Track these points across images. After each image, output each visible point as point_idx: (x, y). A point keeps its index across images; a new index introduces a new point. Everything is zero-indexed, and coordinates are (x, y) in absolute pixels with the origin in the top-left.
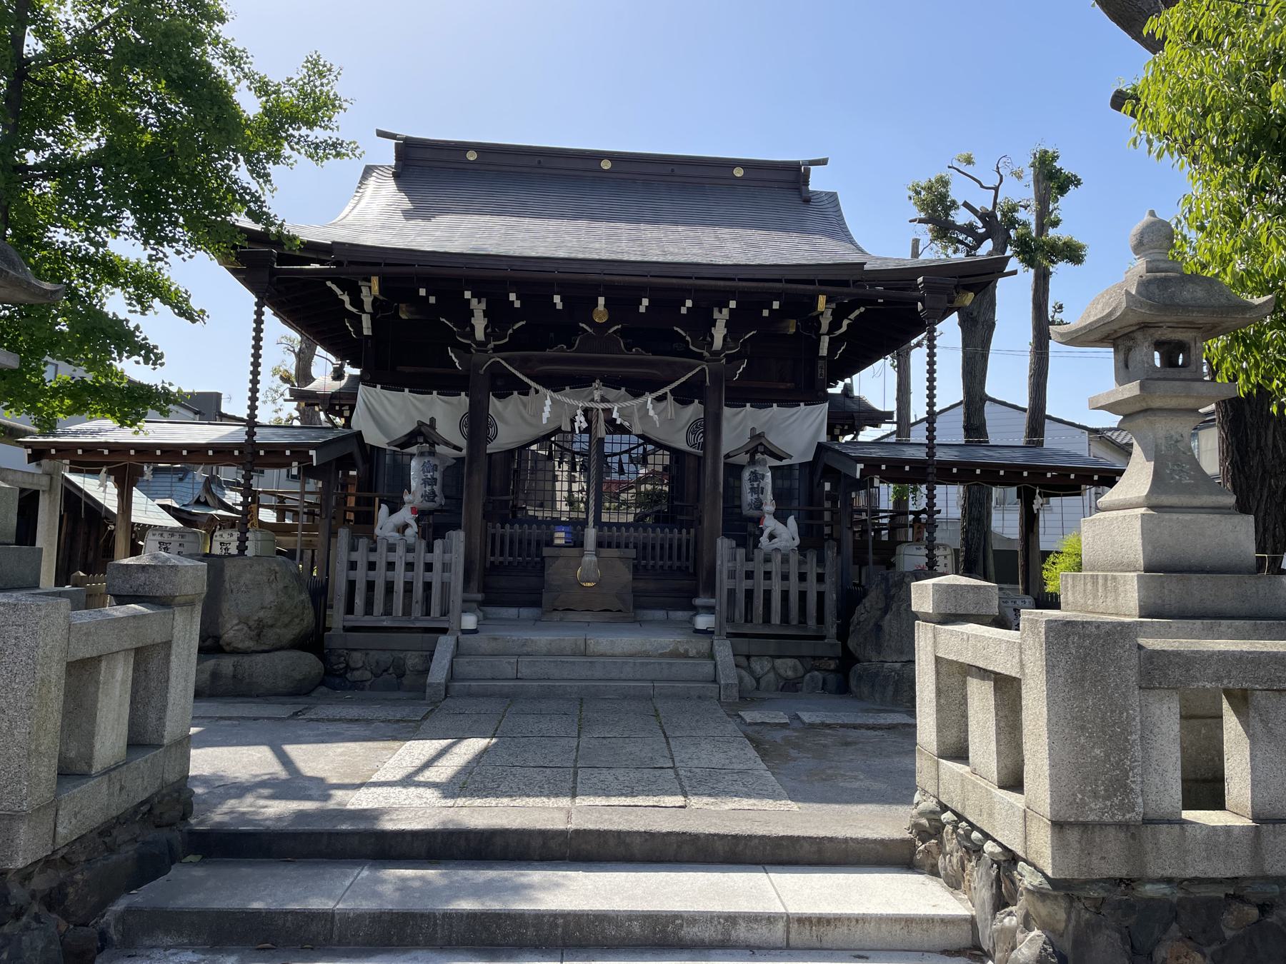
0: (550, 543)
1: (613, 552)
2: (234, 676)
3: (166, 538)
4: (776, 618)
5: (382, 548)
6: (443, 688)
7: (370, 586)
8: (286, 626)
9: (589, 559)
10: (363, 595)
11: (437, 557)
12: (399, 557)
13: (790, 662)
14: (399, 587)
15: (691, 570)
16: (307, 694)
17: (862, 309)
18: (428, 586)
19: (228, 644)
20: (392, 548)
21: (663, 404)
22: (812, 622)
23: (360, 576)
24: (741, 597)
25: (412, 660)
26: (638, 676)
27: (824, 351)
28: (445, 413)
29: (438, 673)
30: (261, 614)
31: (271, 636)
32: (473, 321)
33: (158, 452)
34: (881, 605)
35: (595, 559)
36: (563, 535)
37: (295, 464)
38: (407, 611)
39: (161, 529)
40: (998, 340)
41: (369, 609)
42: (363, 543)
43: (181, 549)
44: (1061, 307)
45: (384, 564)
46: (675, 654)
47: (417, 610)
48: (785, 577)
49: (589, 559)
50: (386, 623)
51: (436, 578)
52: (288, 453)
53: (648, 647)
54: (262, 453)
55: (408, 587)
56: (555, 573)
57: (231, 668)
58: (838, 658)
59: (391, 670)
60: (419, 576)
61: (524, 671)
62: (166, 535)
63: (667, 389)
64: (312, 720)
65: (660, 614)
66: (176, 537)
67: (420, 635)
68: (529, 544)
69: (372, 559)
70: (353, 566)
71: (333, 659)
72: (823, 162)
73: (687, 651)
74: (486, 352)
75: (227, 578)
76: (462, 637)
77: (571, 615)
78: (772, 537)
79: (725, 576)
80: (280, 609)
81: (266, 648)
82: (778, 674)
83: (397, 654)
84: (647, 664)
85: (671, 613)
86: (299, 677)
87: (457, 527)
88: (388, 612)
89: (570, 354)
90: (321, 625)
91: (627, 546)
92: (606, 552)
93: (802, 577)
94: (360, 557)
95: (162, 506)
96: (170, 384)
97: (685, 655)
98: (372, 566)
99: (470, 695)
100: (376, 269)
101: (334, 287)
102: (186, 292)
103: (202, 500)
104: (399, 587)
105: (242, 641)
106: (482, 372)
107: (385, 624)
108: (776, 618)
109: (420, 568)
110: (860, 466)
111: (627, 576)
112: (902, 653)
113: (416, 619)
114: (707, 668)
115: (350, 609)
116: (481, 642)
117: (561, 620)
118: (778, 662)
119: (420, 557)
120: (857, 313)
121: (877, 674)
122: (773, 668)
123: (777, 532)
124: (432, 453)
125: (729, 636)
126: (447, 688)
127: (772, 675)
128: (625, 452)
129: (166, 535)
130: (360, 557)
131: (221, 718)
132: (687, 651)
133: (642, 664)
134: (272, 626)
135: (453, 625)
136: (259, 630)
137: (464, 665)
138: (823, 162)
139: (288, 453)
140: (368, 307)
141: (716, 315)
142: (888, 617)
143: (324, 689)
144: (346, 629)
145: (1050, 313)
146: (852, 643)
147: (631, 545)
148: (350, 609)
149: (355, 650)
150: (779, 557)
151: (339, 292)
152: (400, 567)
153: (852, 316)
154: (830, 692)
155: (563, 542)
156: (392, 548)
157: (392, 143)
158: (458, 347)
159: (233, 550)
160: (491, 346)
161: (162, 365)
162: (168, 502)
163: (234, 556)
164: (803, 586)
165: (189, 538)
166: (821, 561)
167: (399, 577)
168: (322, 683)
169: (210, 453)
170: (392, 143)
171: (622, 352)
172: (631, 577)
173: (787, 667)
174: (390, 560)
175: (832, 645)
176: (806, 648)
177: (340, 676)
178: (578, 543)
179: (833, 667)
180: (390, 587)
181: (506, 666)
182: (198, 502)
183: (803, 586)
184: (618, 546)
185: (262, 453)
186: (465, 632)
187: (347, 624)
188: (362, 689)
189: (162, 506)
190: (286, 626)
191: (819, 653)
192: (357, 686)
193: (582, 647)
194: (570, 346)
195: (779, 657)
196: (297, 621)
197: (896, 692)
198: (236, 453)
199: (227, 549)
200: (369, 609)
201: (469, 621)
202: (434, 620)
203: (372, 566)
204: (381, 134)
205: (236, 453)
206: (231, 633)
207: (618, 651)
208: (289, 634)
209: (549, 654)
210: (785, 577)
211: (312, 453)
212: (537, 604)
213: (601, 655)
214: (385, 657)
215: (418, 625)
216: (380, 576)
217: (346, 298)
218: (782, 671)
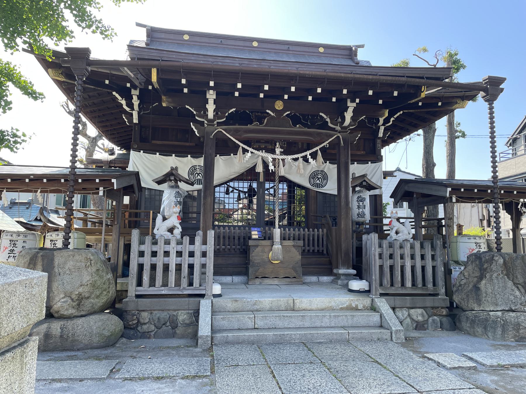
0: (250, 238)
1: (290, 243)
2: (61, 336)
3: (15, 237)
4: (409, 284)
5: (161, 243)
6: (209, 339)
7: (153, 267)
8: (98, 297)
9: (277, 247)
10: (149, 273)
11: (198, 247)
12: (173, 248)
13: (420, 311)
14: (172, 268)
15: (325, 252)
16: (113, 345)
17: (401, 112)
18: (191, 267)
19: (57, 312)
20: (167, 242)
21: (296, 163)
22: (430, 285)
23: (147, 261)
24: (387, 270)
25: (183, 316)
26: (333, 325)
27: (381, 135)
28: (184, 165)
29: (204, 329)
30: (81, 290)
31: (87, 305)
32: (207, 106)
33: (9, 180)
34: (477, 274)
35: (280, 246)
36: (256, 233)
37: (101, 188)
38: (178, 283)
39: (12, 233)
40: (436, 140)
41: (152, 283)
42: (148, 239)
43: (24, 244)
44: (459, 124)
45: (162, 253)
46: (350, 308)
47: (184, 282)
48: (413, 257)
49: (277, 247)
50: (165, 291)
51: (197, 261)
52: (97, 181)
53: (333, 304)
54: (80, 181)
55: (179, 267)
56: (256, 255)
57: (59, 330)
58: (447, 307)
59: (168, 324)
60: (186, 260)
61: (260, 323)
62: (14, 235)
63: (318, 148)
64: (126, 379)
65: (314, 279)
66: (21, 237)
67: (187, 299)
68: (234, 238)
69: (154, 249)
70: (141, 254)
71: (129, 317)
72: (362, 46)
73: (357, 306)
74: (214, 125)
75: (56, 266)
76: (215, 300)
77: (267, 281)
78: (397, 233)
79: (377, 257)
80: (94, 285)
81: (83, 313)
82: (412, 320)
83: (171, 313)
84: (338, 316)
85: (320, 278)
86: (107, 333)
87: (199, 229)
88: (165, 284)
89: (261, 127)
90: (121, 295)
91: (299, 240)
92: (287, 243)
93: (423, 257)
94: (147, 248)
95: (18, 222)
96: (17, 130)
97: (356, 309)
98: (154, 254)
99: (228, 343)
100: (157, 63)
101: (117, 95)
102: (31, 83)
103: (39, 218)
104: (172, 268)
105: (67, 310)
106: (212, 137)
107: (163, 292)
108: (409, 284)
109: (186, 255)
110: (449, 189)
111: (298, 257)
112: (497, 305)
113: (184, 288)
114: (375, 318)
115: (140, 283)
116: (226, 303)
117: (260, 283)
118: (412, 311)
119: (187, 248)
120: (398, 114)
121: (487, 320)
122: (409, 315)
123: (400, 230)
124: (177, 187)
125: (382, 295)
126: (212, 338)
127: (408, 319)
128: (271, 188)
129: (14, 235)
130: (147, 248)
131: (54, 380)
132: (357, 306)
133: (335, 316)
134: (88, 298)
135: (209, 293)
136: (80, 300)
137: (222, 322)
138: (362, 46)
139: (97, 181)
140: (136, 107)
141: (349, 104)
142: (483, 282)
143: (124, 340)
144: (138, 296)
145: (455, 127)
146: (456, 298)
147: (292, 238)
148: (140, 283)
149: (143, 311)
150: (409, 245)
151: (119, 98)
152: (173, 255)
153: (395, 116)
154: (447, 330)
155: (257, 237)
156: (167, 242)
157: (144, 30)
158: (196, 122)
159: (59, 244)
160: (215, 122)
161: (10, 109)
162: (22, 220)
163: (60, 249)
164: (204, 248)
165: (30, 237)
166: (433, 248)
167: (173, 261)
168: (122, 336)
169: (45, 180)
170: (144, 30)
171: (291, 127)
172: (300, 257)
173: (418, 314)
174: (166, 250)
175: (444, 300)
176: (429, 301)
177: (133, 329)
178: (268, 237)
179: (444, 313)
180: (166, 268)
181: (247, 320)
182: (36, 219)
183: (204, 248)
184: (294, 239)
185: (80, 181)
186: (215, 296)
187: (138, 293)
188: (149, 338)
189: (18, 222)
190: (98, 297)
191: (437, 305)
192: (145, 335)
193: (292, 305)
194: (261, 123)
195: (412, 308)
196: (105, 293)
197: (504, 331)
198: (63, 181)
199: (55, 244)
200: (152, 283)
201: (217, 289)
202: (196, 289)
203: (167, 254)
204: (138, 25)
205: (63, 181)
206: (59, 304)
207: (314, 307)
208: (100, 302)
209: (271, 310)
210: (413, 257)
211: (114, 181)
212: (245, 273)
213: (304, 310)
214: (164, 315)
215: (186, 292)
216: (160, 261)
217: (123, 102)
218: (415, 317)
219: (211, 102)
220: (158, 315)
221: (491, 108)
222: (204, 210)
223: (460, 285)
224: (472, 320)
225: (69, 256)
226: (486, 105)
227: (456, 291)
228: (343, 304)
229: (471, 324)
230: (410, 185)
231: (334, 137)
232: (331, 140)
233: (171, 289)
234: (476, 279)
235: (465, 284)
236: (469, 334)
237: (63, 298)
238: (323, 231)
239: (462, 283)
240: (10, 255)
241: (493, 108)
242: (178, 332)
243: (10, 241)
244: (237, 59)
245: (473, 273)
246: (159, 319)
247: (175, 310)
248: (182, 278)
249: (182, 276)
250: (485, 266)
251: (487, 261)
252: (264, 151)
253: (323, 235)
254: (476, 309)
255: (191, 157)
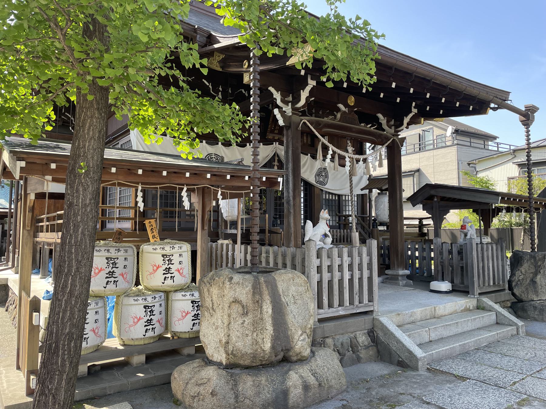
34: (533, 270)
50: (341, 312)
79: (314, 254)
114: (491, 317)
142: (539, 277)
202: (366, 306)
219: (308, 88)
220: (341, 340)
221: (528, 132)
222: (294, 211)
223: (519, 280)
224: (541, 309)
225: (289, 280)
226: (523, 129)
227: (515, 286)
228: (462, 307)
229: (540, 312)
230: (440, 190)
231: (391, 141)
232: (389, 142)
233: (347, 308)
234: (531, 275)
235: (523, 279)
236: (536, 320)
237: (301, 335)
238: (344, 232)
239: (520, 278)
240: (110, 280)
241: (529, 131)
242: (361, 356)
243: (107, 259)
244: (389, 51)
245: (529, 269)
246: (342, 344)
247: (352, 333)
248: (355, 295)
249: (355, 293)
250: (539, 264)
251: (540, 260)
252: (277, 143)
253: (344, 236)
254: (535, 299)
255: (206, 143)
